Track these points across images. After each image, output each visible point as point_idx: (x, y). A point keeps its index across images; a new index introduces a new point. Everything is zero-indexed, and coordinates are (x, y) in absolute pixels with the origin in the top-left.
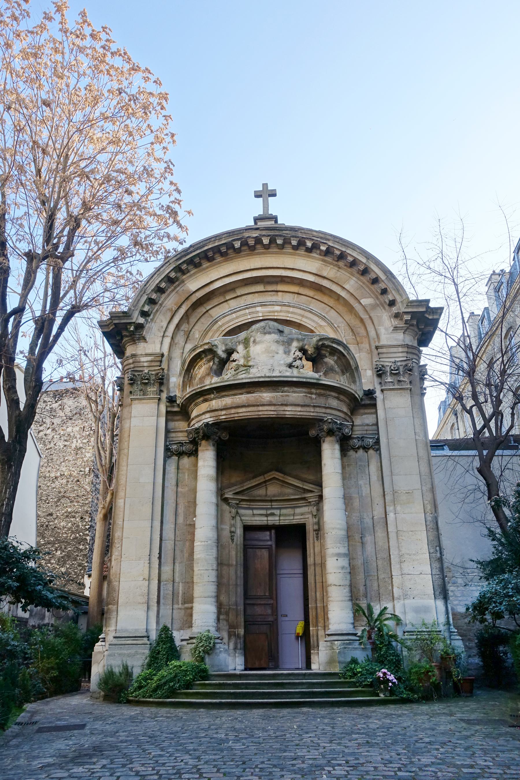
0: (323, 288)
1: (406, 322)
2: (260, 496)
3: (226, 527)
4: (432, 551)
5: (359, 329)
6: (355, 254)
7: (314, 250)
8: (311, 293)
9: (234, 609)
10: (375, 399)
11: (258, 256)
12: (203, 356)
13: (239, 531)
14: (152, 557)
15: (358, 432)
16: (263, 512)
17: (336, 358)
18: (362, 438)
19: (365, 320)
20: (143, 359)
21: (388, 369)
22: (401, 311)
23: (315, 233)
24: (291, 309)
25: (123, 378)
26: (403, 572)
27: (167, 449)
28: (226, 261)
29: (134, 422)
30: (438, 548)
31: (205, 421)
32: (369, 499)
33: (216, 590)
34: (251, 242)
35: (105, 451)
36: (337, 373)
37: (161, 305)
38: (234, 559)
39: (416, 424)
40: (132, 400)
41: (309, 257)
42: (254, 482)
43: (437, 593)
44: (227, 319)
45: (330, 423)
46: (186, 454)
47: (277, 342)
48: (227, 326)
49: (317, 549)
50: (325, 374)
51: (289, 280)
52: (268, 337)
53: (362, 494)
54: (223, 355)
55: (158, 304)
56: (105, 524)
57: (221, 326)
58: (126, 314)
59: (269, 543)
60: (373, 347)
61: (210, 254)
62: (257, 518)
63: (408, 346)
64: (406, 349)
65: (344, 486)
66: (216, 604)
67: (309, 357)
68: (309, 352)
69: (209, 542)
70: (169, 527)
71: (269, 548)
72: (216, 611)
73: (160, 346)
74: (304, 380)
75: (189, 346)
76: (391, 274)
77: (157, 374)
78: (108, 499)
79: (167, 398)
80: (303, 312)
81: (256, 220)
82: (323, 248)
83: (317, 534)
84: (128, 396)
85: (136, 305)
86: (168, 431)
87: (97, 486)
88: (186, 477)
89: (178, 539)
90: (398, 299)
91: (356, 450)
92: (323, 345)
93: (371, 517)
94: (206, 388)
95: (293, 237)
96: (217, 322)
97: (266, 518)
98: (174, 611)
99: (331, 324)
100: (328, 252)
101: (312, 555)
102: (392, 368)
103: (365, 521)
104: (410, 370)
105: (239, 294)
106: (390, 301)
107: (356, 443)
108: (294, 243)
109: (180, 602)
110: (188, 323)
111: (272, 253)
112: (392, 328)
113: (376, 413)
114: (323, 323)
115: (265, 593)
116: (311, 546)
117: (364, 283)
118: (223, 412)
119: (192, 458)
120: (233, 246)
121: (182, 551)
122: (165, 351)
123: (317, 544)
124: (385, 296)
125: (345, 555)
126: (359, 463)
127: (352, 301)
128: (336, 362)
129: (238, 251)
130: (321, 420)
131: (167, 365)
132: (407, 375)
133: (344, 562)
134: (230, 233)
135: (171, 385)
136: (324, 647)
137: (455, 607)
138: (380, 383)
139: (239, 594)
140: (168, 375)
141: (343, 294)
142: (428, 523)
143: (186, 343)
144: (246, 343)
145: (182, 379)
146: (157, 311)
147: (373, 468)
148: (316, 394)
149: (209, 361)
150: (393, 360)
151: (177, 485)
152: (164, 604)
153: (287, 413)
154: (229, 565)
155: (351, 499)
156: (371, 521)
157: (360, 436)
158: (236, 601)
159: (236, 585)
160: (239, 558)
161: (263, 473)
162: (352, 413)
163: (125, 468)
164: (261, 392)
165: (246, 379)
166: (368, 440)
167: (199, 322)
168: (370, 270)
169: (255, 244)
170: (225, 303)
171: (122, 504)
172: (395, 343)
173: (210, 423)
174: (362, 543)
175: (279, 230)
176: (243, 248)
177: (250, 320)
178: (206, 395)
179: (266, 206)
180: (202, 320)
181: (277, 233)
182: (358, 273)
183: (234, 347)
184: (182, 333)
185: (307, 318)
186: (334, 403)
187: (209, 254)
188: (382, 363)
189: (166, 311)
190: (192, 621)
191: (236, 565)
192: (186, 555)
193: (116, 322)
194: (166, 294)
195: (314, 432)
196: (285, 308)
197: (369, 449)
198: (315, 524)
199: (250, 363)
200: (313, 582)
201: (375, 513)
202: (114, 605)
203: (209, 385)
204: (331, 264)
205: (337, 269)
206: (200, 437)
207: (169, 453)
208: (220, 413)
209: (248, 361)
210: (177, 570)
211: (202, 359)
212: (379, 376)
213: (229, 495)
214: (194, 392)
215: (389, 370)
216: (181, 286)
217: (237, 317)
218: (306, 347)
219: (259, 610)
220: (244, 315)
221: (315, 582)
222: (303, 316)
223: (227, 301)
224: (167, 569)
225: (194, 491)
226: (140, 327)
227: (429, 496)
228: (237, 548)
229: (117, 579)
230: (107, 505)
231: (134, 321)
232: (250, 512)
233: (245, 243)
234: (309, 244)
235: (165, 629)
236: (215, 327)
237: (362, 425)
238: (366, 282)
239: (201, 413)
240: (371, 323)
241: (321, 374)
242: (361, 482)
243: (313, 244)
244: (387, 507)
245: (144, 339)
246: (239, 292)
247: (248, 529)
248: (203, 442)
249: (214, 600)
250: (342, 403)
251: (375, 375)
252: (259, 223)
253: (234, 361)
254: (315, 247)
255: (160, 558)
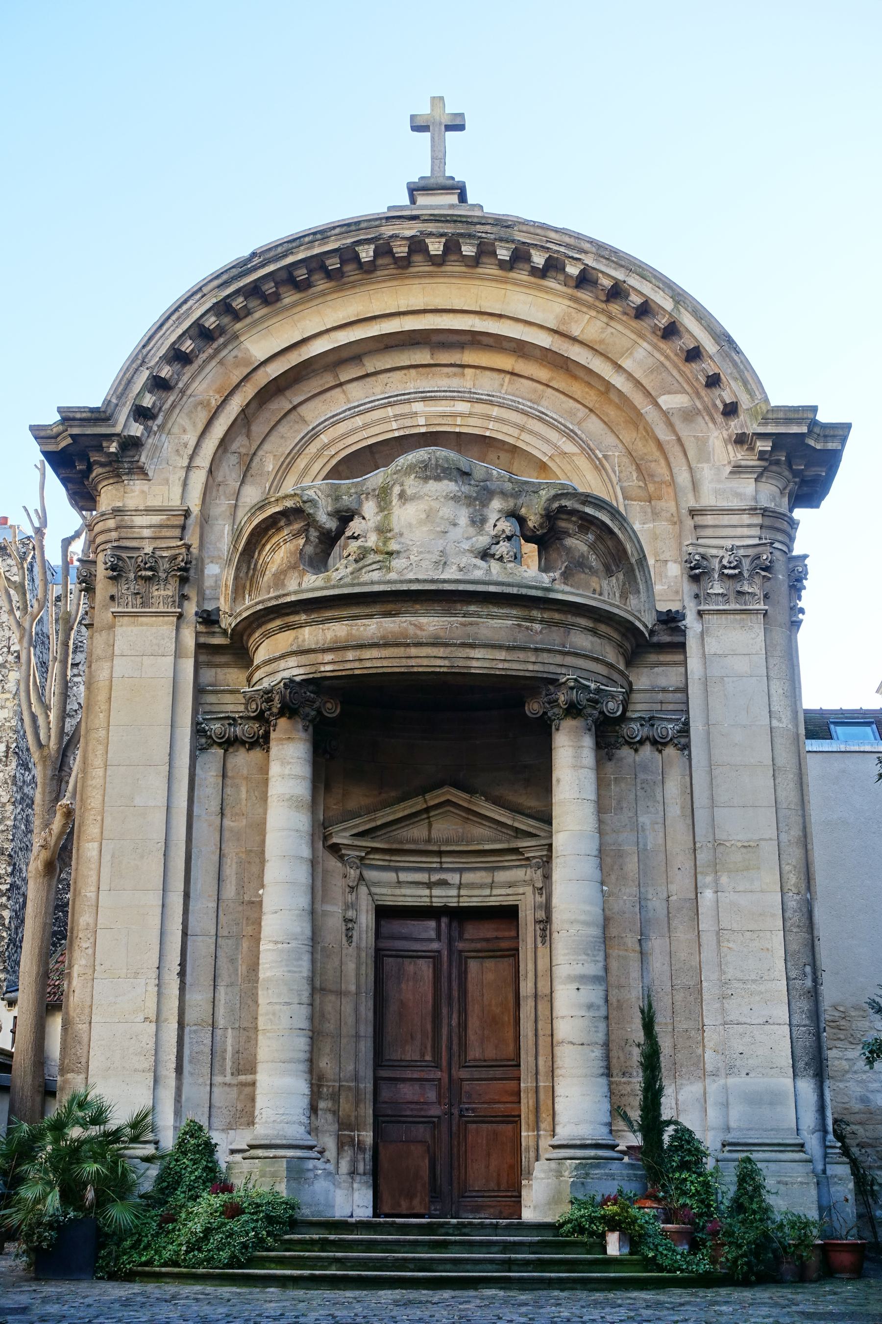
0: (571, 366)
1: (762, 456)
2: (414, 841)
3: (335, 911)
4: (793, 974)
5: (653, 465)
6: (647, 289)
7: (552, 273)
8: (543, 374)
9: (349, 1088)
10: (683, 633)
11: (417, 281)
12: (282, 523)
13: (366, 919)
14: (165, 971)
15: (640, 707)
16: (422, 877)
17: (591, 537)
18: (651, 720)
19: (667, 447)
20: (139, 520)
21: (716, 564)
22: (750, 431)
23: (553, 235)
24: (495, 411)
25: (94, 562)
26: (728, 1019)
27: (198, 731)
28: (340, 288)
29: (121, 666)
30: (808, 969)
31: (287, 674)
32: (662, 856)
33: (307, 1048)
34: (401, 250)
35: (46, 708)
36: (593, 571)
37: (183, 392)
38: (353, 980)
39: (773, 692)
40: (115, 615)
41: (540, 288)
42: (401, 811)
43: (801, 1065)
44: (342, 428)
45: (572, 688)
46: (243, 743)
47: (455, 499)
48: (341, 445)
49: (542, 964)
50: (566, 576)
51: (490, 341)
52: (432, 485)
53: (645, 845)
54: (331, 524)
55: (177, 391)
56: (49, 885)
57: (326, 447)
58: (99, 416)
59: (435, 946)
60: (684, 512)
61: (301, 274)
62: (408, 891)
63: (765, 512)
64: (758, 520)
65: (601, 830)
66: (307, 1076)
67: (529, 533)
68: (531, 524)
69: (294, 944)
70: (204, 905)
71: (435, 958)
72: (307, 1091)
73: (180, 490)
74: (515, 591)
75: (252, 494)
76: (730, 341)
77: (175, 557)
78: (57, 824)
79: (197, 614)
80: (525, 418)
81: (414, 190)
82: (573, 270)
83: (544, 930)
84: (106, 607)
85: (122, 394)
86: (199, 690)
87: (26, 790)
88: (244, 795)
89: (223, 932)
90: (745, 402)
91: (636, 745)
92: (562, 509)
93: (665, 895)
94: (288, 599)
95: (501, 240)
96: (317, 435)
97: (427, 892)
98: (215, 1089)
99: (588, 451)
100: (585, 280)
101: (531, 975)
102: (725, 562)
103: (650, 905)
104: (766, 569)
105: (371, 370)
106: (726, 405)
107: (636, 730)
108: (503, 254)
109: (229, 1071)
110: (248, 436)
111: (452, 275)
112: (728, 469)
113: (685, 663)
114: (569, 447)
115: (423, 1055)
116: (530, 955)
117: (667, 357)
118: (329, 657)
119: (257, 754)
120: (357, 257)
121: (232, 961)
122: (194, 503)
123: (542, 951)
124: (717, 392)
125: (596, 979)
126: (642, 776)
127: (638, 399)
128: (592, 547)
129: (368, 269)
130: (554, 682)
131: (197, 536)
132: (757, 580)
133: (593, 994)
134: (348, 225)
135: (208, 583)
136: (544, 1171)
137: (871, 1096)
138: (697, 596)
139: (362, 1055)
140: (201, 560)
141: (618, 381)
142: (788, 914)
143: (243, 482)
144: (383, 496)
145: (232, 573)
146: (173, 406)
147: (673, 787)
148: (541, 622)
149: (296, 536)
150: (728, 543)
151: (222, 814)
152: (191, 1074)
153: (475, 664)
154: (340, 993)
155: (621, 856)
156: (665, 904)
157: (647, 716)
158: (356, 1072)
159: (357, 1036)
160: (363, 979)
161: (423, 791)
162: (629, 663)
163: (100, 772)
164: (415, 613)
165: (379, 583)
166: (665, 724)
167: (275, 433)
168: (682, 329)
169: (411, 252)
170: (338, 390)
171: (95, 853)
172: (735, 503)
173: (298, 679)
174: (641, 953)
175: (467, 223)
176: (380, 262)
177: (396, 434)
178: (288, 614)
179: (438, 158)
180: (282, 429)
181: (461, 229)
182: (654, 333)
183: (354, 506)
184: (233, 459)
185: (531, 432)
186: (582, 641)
187: (297, 273)
188: (701, 550)
189: (196, 407)
190: (253, 1112)
191: (358, 994)
192: (242, 969)
193: (76, 431)
194: (195, 366)
195: (536, 706)
196: (479, 408)
197: (665, 744)
198: (540, 907)
199: (393, 546)
200: (531, 1035)
201: (673, 888)
202: (78, 1073)
203: (296, 593)
204: (591, 307)
205: (605, 319)
206: (275, 710)
207: (203, 740)
208: (320, 657)
209: (386, 541)
210: (223, 1002)
211: (279, 529)
212: (695, 579)
213: (341, 838)
214: (260, 607)
215: (717, 567)
216: (230, 347)
217: (366, 426)
218: (523, 511)
219: (408, 1092)
220: (385, 420)
221: (536, 1035)
222: (522, 428)
223: (341, 385)
224: (198, 998)
225: (260, 828)
226: (132, 444)
227: (794, 855)
228: (359, 956)
229: (85, 1018)
230: (52, 841)
231: (118, 429)
232: (391, 876)
233: (384, 250)
234: (539, 259)
235: (195, 1130)
236: (313, 448)
237: (652, 691)
238: (672, 355)
239: (277, 654)
240: (680, 455)
241: (557, 575)
242: (644, 819)
243: (547, 260)
244: (699, 877)
245: (143, 472)
246: (371, 364)
247: (384, 913)
248: (283, 722)
249: (303, 1067)
250: (605, 641)
251: (685, 577)
252: (422, 200)
253: (355, 538)
254: (553, 267)
255: (182, 974)
